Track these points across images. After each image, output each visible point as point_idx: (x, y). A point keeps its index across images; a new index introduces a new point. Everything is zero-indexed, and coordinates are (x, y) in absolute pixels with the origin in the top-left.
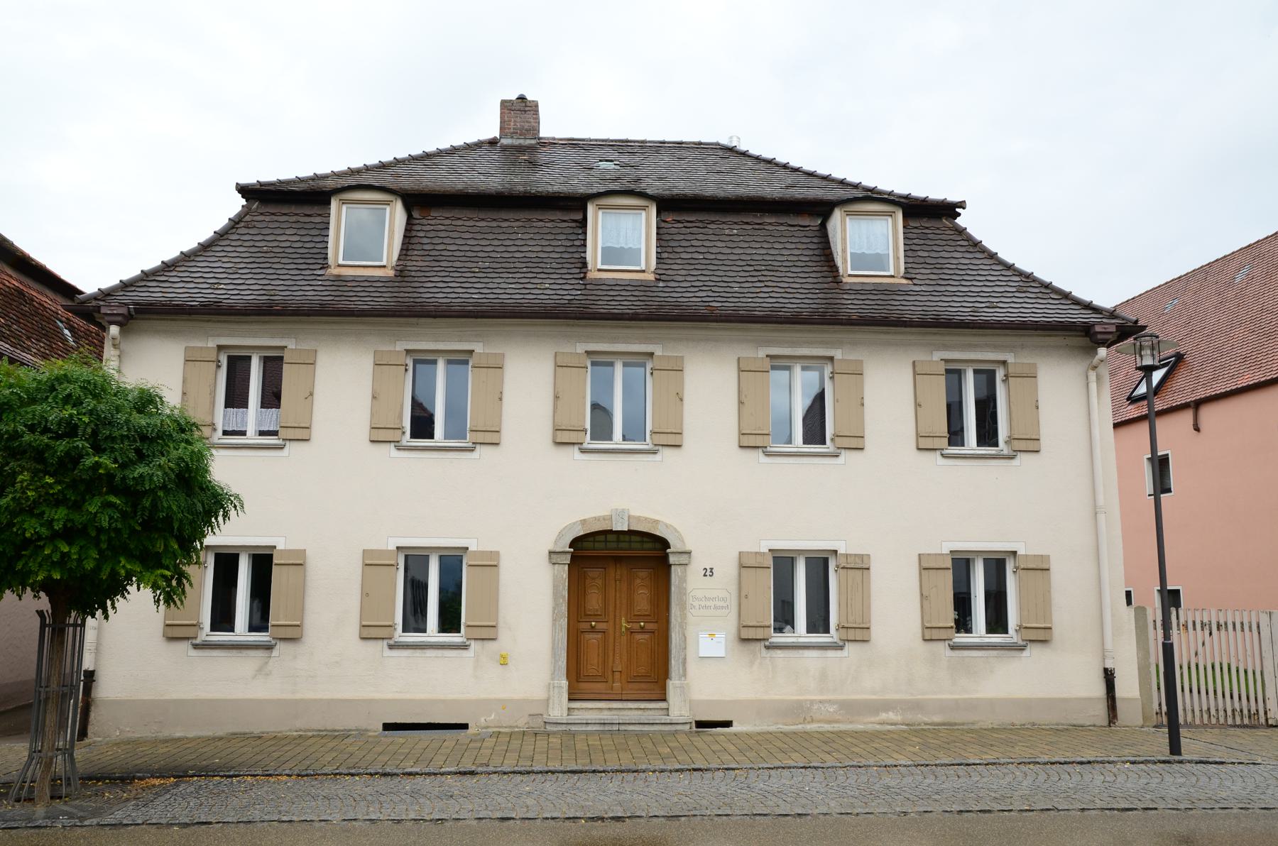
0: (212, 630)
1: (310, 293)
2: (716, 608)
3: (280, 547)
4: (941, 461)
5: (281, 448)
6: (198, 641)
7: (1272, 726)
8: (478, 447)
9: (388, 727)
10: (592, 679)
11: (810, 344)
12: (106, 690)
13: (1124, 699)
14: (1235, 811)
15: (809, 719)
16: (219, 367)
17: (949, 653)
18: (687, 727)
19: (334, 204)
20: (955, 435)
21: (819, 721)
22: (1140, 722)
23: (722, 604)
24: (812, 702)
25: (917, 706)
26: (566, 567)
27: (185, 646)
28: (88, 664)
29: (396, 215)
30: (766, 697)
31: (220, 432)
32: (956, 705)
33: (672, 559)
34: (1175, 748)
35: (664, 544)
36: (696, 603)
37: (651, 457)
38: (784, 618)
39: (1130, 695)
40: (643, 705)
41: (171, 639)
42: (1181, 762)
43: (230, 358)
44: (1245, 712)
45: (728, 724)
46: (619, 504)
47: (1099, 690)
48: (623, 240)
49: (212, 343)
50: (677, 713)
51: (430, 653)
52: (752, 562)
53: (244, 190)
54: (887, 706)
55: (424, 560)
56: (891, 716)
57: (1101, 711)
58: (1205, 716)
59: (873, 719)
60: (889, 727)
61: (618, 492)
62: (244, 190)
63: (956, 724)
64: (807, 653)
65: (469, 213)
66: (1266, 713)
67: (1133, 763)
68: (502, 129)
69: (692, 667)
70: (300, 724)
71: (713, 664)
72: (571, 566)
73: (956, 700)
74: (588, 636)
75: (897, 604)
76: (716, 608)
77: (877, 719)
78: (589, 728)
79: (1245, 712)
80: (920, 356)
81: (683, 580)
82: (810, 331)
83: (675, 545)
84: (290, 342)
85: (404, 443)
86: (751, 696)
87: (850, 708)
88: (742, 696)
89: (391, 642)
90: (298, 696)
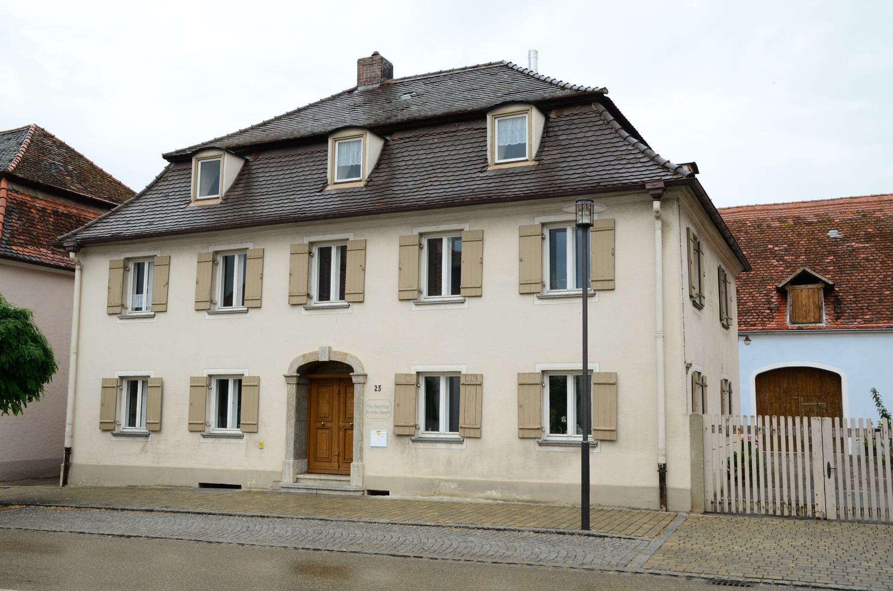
0: (427, 429)
1: (478, 185)
2: (382, 413)
3: (464, 372)
4: (538, 302)
5: (463, 302)
6: (115, 432)
7: (819, 518)
8: (467, 299)
9: (203, 485)
10: (323, 460)
11: (447, 221)
12: (78, 458)
13: (675, 489)
14: (629, 574)
15: (437, 493)
16: (543, 239)
17: (538, 448)
18: (360, 494)
19: (330, 141)
20: (435, 288)
21: (444, 495)
22: (689, 509)
23: (384, 410)
24: (440, 480)
25: (511, 487)
26: (294, 386)
27: (109, 434)
28: (67, 444)
29: (535, 121)
30: (411, 476)
31: (130, 309)
32: (542, 487)
33: (354, 380)
34: (586, 524)
35: (350, 369)
36: (370, 410)
37: (345, 311)
38: (432, 421)
39: (682, 486)
40: (339, 478)
41: (104, 431)
42: (589, 535)
43: (430, 241)
44: (794, 505)
45: (387, 493)
46: (325, 343)
47: (655, 482)
48: (517, 135)
49: (538, 220)
50: (355, 484)
51: (224, 441)
52: (403, 381)
53: (165, 157)
54: (491, 486)
55: (565, 379)
56: (494, 493)
57: (655, 496)
58: (756, 507)
59: (481, 495)
60: (304, 491)
61: (326, 334)
62: (165, 157)
63: (540, 502)
64: (439, 446)
65: (280, 154)
66: (813, 507)
67: (536, 532)
68: (358, 80)
69: (367, 454)
70: (160, 482)
71: (380, 452)
72: (298, 384)
73: (541, 484)
74: (320, 431)
75: (500, 410)
76: (382, 413)
77: (484, 495)
78: (300, 491)
79: (794, 505)
80: (525, 222)
81: (362, 393)
82: (445, 213)
83: (357, 370)
84: (601, 213)
85: (545, 294)
86: (402, 475)
87: (465, 486)
88: (395, 474)
89: (540, 441)
90: (160, 465)
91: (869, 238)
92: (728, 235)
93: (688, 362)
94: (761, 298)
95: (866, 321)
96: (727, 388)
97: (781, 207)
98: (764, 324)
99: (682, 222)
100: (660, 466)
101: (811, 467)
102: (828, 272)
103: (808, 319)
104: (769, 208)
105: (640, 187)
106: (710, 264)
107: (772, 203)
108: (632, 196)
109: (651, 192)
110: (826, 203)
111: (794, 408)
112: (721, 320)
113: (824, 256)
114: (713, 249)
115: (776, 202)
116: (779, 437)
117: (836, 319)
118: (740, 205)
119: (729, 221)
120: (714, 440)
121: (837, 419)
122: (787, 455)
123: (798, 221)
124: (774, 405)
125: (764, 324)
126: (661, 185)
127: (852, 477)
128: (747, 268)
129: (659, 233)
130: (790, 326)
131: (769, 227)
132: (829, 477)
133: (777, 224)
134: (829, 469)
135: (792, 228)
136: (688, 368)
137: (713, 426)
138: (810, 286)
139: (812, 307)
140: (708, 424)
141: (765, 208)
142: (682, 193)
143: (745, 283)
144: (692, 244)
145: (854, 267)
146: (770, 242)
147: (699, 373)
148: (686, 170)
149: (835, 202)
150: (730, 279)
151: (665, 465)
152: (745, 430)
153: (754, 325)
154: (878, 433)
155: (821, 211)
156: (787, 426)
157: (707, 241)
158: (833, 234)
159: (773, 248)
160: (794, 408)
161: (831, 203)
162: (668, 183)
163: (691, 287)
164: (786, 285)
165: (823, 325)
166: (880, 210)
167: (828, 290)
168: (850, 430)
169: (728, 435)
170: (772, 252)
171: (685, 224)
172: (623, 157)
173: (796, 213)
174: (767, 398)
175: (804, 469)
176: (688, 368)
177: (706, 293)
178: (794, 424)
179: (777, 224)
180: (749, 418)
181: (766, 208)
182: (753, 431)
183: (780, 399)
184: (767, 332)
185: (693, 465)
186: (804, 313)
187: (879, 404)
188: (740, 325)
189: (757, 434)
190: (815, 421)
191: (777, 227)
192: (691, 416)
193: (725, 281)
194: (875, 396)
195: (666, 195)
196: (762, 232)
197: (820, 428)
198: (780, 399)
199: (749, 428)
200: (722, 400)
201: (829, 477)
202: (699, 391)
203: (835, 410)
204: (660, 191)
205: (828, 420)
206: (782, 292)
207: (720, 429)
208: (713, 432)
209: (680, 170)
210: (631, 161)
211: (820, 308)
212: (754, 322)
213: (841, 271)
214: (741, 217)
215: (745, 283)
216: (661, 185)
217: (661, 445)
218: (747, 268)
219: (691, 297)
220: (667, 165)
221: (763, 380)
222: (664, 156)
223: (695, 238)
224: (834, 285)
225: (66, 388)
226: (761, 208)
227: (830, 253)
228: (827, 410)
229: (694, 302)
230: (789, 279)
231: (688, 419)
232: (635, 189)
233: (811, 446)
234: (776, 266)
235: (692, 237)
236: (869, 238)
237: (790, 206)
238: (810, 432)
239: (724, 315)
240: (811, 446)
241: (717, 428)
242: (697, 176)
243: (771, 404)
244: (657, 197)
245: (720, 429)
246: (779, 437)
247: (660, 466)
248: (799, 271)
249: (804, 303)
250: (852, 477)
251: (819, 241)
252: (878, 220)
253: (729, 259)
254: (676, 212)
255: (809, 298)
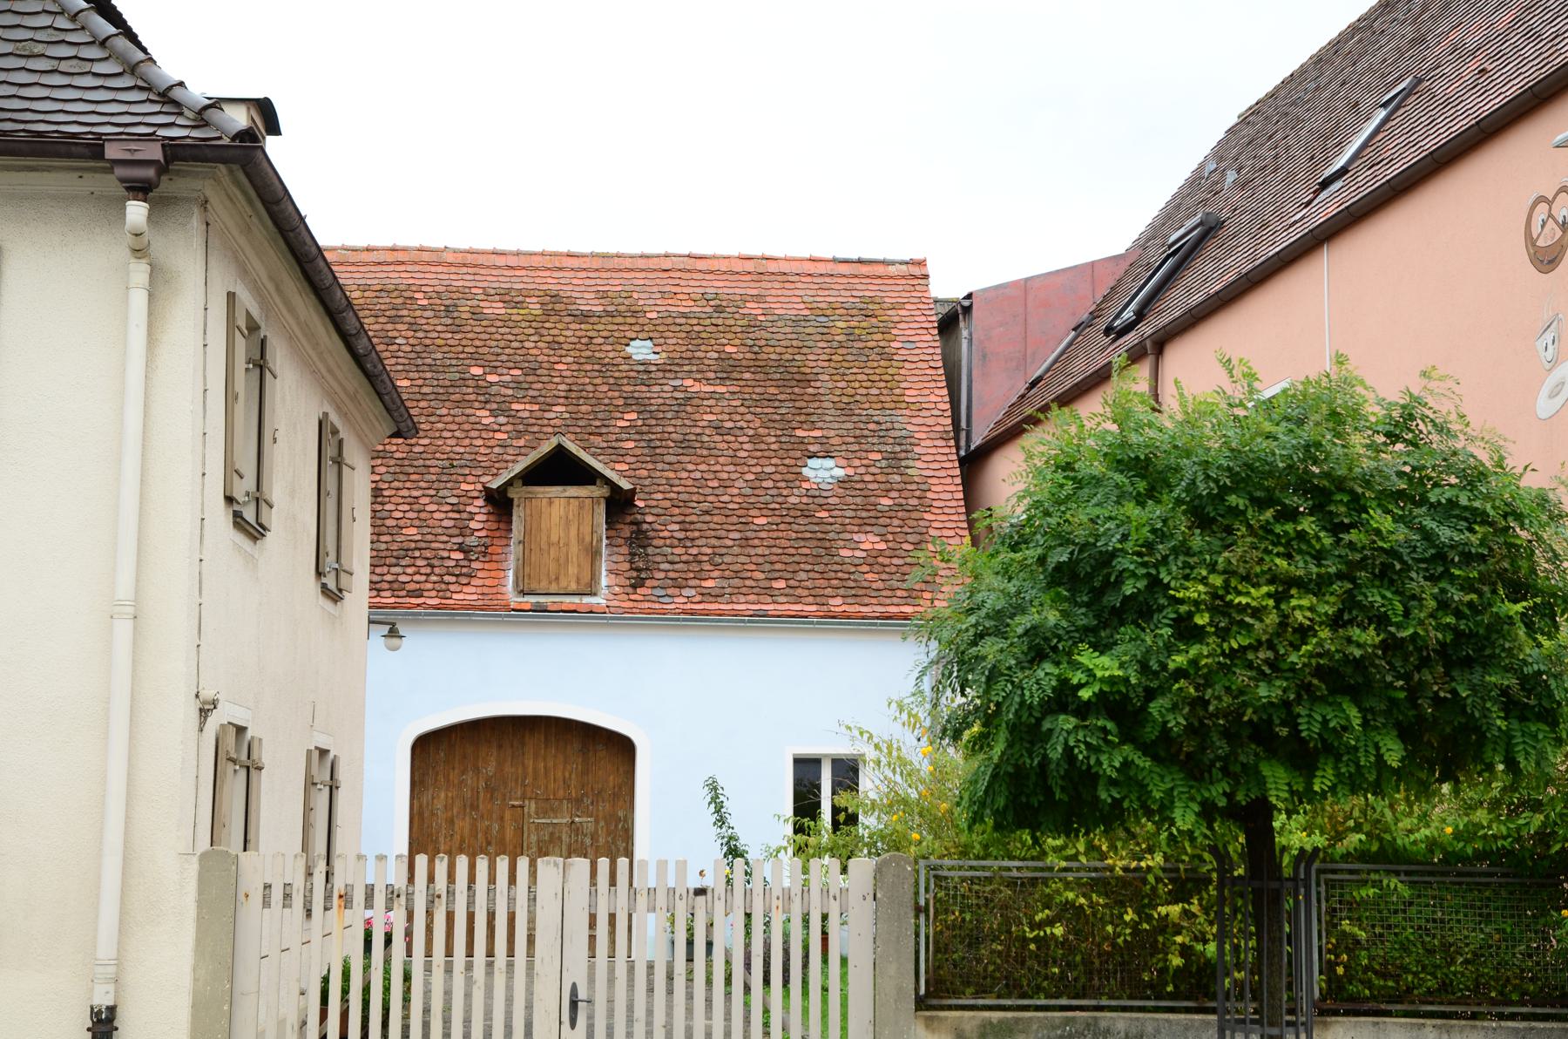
91: (727, 370)
92: (351, 325)
93: (207, 694)
94: (442, 517)
95: (707, 595)
96: (324, 775)
97: (513, 261)
98: (443, 593)
99: (215, 273)
100: (95, 1013)
101: (530, 992)
102: (621, 455)
103: (563, 583)
104: (481, 260)
105: (83, 151)
106: (297, 407)
107: (489, 247)
108: (61, 176)
109: (121, 171)
110: (628, 264)
111: (509, 833)
112: (319, 573)
113: (613, 410)
114: (310, 368)
115: (575, 249)
116: (450, 917)
117: (634, 587)
118: (401, 243)
119: (365, 288)
120: (267, 928)
121: (623, 862)
122: (469, 967)
123: (554, 305)
124: (458, 824)
125: (443, 593)
126: (154, 152)
127: (630, 1020)
128: (403, 429)
129: (139, 299)
130: (514, 600)
131: (476, 314)
132: (573, 1024)
133: (498, 309)
134: (574, 1005)
135: (537, 325)
136: (204, 713)
137: (267, 887)
138: (572, 491)
139: (574, 548)
140: (252, 883)
141: (470, 259)
142: (218, 187)
143: (402, 471)
144: (240, 343)
145: (684, 445)
146: (476, 358)
147: (241, 730)
148: (239, 119)
149: (652, 264)
150: (356, 456)
151: (112, 1010)
152: (359, 897)
153: (418, 593)
154: (701, 899)
155: (615, 285)
156: (479, 883)
157: (291, 338)
158: (641, 350)
159: (482, 378)
160: (509, 833)
161: (641, 264)
162: (176, 152)
163: (232, 471)
164: (510, 483)
165: (599, 601)
166: (758, 298)
167: (619, 504)
168: (651, 892)
169: (309, 913)
170: (481, 387)
171: (224, 280)
172: (39, 49)
173: (551, 283)
174: (439, 805)
175: (509, 1000)
176: (204, 713)
177: (277, 491)
178: (492, 880)
179: (498, 309)
180: (371, 862)
181: (471, 261)
182: (380, 899)
183: (474, 807)
184: (450, 614)
185: (200, 1007)
186: (552, 566)
187: (721, 821)
188: (375, 587)
189: (389, 909)
190: (549, 868)
191: (498, 317)
192: (204, 857)
193: (339, 462)
194: (714, 799)
195: (166, 186)
196: (456, 328)
197: (560, 886)
198: (474, 807)
199: (370, 892)
200: (308, 810)
201: (573, 1024)
202: (235, 785)
203: (613, 837)
204: (150, 173)
205: (581, 865)
206: (500, 503)
207: (287, 896)
208: (266, 903)
209: (213, 115)
210: (64, 66)
211: (594, 554)
212: (415, 584)
213: (654, 453)
214: (397, 277)
215: (402, 471)
216: (154, 152)
217: (106, 950)
218: (403, 429)
219: (229, 500)
220: (177, 94)
221: (427, 747)
222: (170, 65)
223: (253, 327)
224: (633, 492)
225: (819, 787)
226: (459, 259)
227: (631, 402)
228: (594, 837)
229: (237, 515)
230: (518, 468)
231: (194, 867)
232: (69, 156)
233: (531, 940)
234: (487, 428)
235: (242, 322)
236: (727, 370)
237: (536, 261)
238: (532, 900)
239: (330, 561)
240: (531, 940)
241: (277, 895)
242: (271, 144)
243: (451, 822)
244: (141, 190)
245: (287, 896)
246: (450, 917)
247: (95, 1013)
248: (546, 447)
249: (554, 538)
250: (630, 1020)
251: (605, 367)
252: (753, 325)
253: (353, 398)
254: (197, 242)
255: (568, 523)
